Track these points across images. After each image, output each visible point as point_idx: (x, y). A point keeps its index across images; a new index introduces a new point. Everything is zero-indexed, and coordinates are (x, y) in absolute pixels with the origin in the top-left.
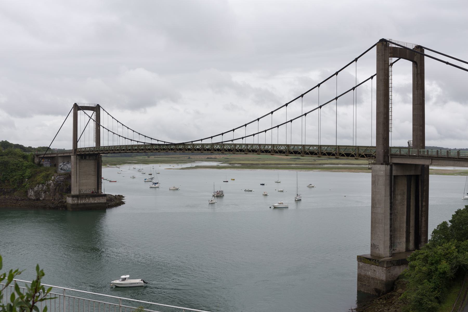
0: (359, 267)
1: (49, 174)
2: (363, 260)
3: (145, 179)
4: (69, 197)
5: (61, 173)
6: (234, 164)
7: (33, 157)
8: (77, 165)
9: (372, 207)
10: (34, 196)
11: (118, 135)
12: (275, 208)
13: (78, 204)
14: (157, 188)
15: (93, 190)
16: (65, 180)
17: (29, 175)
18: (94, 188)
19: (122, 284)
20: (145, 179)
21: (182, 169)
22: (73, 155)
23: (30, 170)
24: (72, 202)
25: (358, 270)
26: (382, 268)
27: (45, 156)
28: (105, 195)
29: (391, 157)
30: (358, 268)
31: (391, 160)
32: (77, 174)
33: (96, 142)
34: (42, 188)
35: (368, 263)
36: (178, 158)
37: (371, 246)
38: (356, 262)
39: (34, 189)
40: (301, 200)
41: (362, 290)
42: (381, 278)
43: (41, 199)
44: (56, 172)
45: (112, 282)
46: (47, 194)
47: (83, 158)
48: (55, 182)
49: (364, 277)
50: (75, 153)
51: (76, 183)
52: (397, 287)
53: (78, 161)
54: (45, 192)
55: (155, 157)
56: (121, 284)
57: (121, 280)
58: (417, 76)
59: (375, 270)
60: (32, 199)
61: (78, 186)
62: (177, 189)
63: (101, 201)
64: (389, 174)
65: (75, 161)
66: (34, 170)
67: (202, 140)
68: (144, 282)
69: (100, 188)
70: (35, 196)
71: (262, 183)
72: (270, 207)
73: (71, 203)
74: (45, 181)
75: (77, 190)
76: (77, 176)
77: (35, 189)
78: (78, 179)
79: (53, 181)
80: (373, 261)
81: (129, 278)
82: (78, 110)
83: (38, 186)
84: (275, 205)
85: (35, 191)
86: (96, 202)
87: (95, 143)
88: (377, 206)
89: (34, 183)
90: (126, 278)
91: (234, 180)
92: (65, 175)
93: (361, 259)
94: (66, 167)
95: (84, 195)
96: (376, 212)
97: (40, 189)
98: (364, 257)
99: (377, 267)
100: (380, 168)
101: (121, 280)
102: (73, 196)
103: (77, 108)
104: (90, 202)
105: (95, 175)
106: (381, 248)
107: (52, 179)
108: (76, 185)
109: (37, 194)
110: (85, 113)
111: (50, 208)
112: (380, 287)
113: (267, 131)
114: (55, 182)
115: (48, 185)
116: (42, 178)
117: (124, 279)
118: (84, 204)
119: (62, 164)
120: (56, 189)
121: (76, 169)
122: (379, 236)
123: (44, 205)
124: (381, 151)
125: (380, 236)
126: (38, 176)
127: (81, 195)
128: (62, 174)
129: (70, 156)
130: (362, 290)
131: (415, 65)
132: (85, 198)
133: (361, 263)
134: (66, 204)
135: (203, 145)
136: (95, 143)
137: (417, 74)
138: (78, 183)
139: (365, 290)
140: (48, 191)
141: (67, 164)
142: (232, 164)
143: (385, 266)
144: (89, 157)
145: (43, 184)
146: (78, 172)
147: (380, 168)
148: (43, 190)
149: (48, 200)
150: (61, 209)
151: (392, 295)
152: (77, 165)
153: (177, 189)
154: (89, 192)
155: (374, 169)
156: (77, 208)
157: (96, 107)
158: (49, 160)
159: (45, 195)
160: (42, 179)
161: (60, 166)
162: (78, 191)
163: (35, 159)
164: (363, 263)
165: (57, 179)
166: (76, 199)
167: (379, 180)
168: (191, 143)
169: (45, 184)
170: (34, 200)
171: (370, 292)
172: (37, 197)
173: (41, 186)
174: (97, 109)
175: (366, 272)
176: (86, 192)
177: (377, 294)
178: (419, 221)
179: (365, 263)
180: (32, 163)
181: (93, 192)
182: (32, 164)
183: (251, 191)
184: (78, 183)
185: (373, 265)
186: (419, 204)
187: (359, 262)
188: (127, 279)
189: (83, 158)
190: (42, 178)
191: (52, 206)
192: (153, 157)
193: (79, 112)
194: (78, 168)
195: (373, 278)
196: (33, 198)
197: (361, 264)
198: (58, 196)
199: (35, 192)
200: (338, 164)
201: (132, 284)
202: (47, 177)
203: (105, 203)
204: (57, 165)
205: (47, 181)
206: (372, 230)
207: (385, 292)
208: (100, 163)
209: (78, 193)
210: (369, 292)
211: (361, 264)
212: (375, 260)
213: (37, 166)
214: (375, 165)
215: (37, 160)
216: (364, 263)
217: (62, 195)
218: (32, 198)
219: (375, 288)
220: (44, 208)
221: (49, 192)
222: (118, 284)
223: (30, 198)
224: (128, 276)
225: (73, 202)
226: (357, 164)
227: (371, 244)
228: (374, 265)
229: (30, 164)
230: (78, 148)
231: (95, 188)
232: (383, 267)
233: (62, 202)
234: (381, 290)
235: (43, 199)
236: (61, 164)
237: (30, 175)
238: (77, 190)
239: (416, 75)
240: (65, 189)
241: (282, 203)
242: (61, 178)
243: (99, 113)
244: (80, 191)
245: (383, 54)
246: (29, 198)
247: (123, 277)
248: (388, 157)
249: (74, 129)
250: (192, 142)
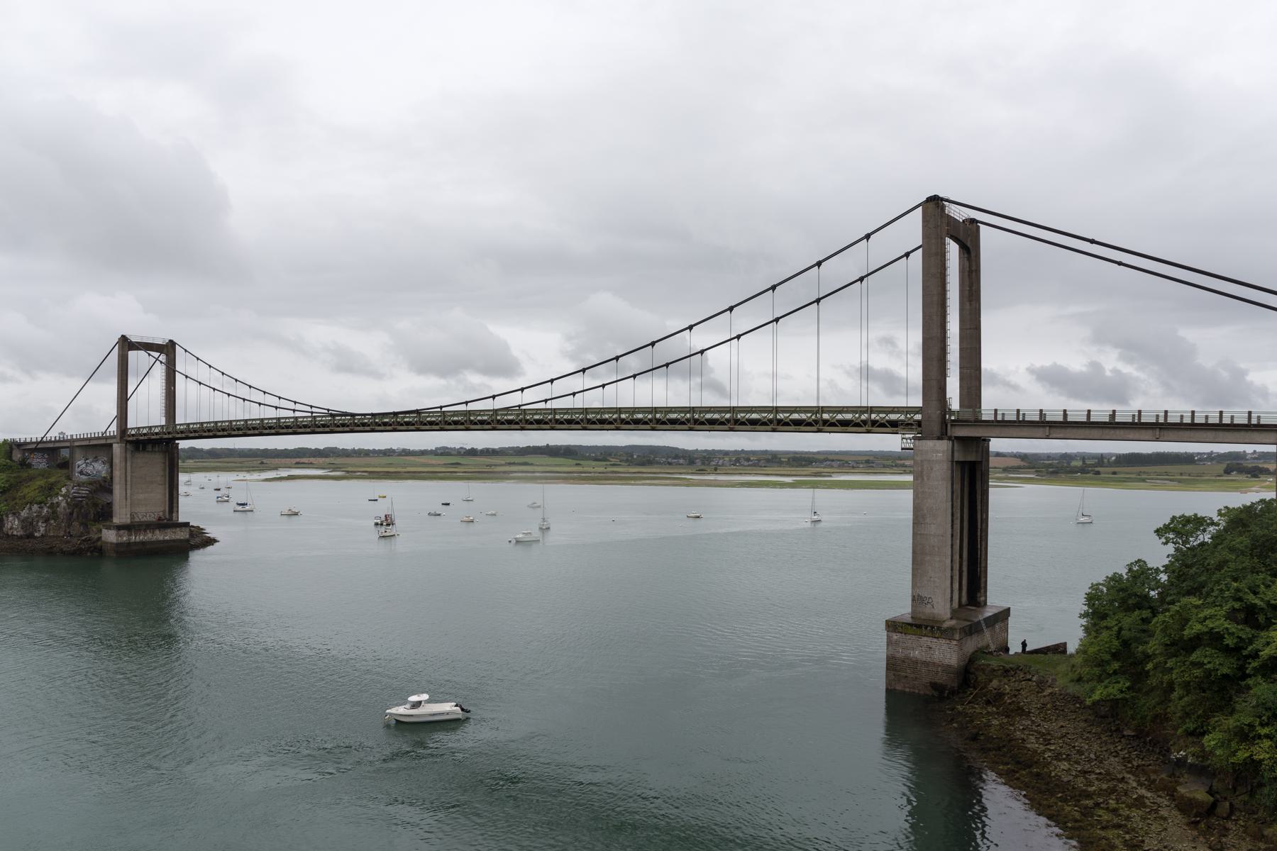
0: (890, 642)
1: (55, 482)
2: (902, 627)
3: (218, 498)
4: (108, 528)
5: (81, 480)
6: (355, 472)
7: (8, 448)
9: (913, 523)
12: (518, 542)
13: (129, 544)
14: (248, 513)
15: (161, 514)
16: (90, 495)
17: (3, 485)
18: (162, 509)
19: (412, 715)
20: (218, 498)
21: (267, 480)
22: (118, 443)
23: (5, 475)
24: (117, 540)
25: (887, 649)
26: (948, 642)
27: (40, 446)
28: (186, 525)
29: (952, 425)
30: (888, 645)
31: (951, 430)
32: (126, 481)
33: (166, 417)
34: (40, 512)
35: (912, 634)
36: (241, 463)
37: (913, 600)
38: (883, 635)
40: (549, 528)
41: (897, 688)
42: (946, 662)
43: (36, 534)
44: (69, 478)
45: (388, 711)
46: (51, 525)
47: (141, 449)
48: (69, 500)
49: (904, 661)
50: (121, 438)
51: (124, 500)
52: (977, 678)
53: (129, 455)
54: (47, 520)
55: (195, 462)
56: (409, 716)
57: (408, 706)
58: (969, 275)
59: (931, 646)
60: (14, 535)
61: (129, 506)
62: (296, 514)
63: (178, 537)
64: (950, 458)
65: (124, 455)
66: (15, 475)
67: (467, 403)
68: (462, 710)
69: (175, 509)
70: (22, 528)
71: (444, 502)
72: (510, 541)
73: (115, 541)
74: (46, 498)
75: (126, 514)
76: (126, 484)
77: (22, 514)
78: (129, 491)
79: (64, 496)
80: (926, 628)
81: (428, 701)
82: (129, 350)
83: (30, 509)
84: (518, 536)
85: (22, 518)
86: (167, 538)
87: (164, 419)
88: (928, 520)
89: (17, 501)
90: (420, 702)
91: (385, 497)
92: (91, 484)
93: (892, 626)
94: (91, 468)
95: (141, 525)
96: (926, 533)
97: (35, 514)
98: (903, 623)
99: (935, 640)
100: (935, 445)
101: (408, 706)
102: (119, 528)
103: (126, 345)
104: (154, 538)
105: (165, 484)
106: (938, 602)
108: (124, 504)
109: (28, 524)
110: (149, 355)
111: (63, 552)
112: (942, 678)
113: (577, 395)
114: (69, 500)
115: (53, 507)
116: (37, 491)
117: (417, 705)
118: (143, 543)
119: (83, 461)
120: (71, 514)
121: (124, 471)
122: (932, 579)
123: (49, 546)
124: (935, 413)
125: (936, 579)
126: (26, 487)
127: (136, 524)
128: (84, 483)
129: (111, 445)
130: (899, 687)
131: (966, 256)
132: (145, 531)
133: (894, 634)
134: (99, 543)
135: (470, 413)
136: (164, 418)
137: (969, 272)
138: (129, 500)
139: (905, 687)
140: (53, 519)
141: (93, 462)
142: (352, 472)
143: (957, 637)
144: (153, 446)
145: (40, 503)
146: (129, 478)
147: (935, 445)
148: (42, 517)
149: (54, 536)
150: (89, 554)
151: (1000, 693)
152: (126, 463)
153: (296, 514)
154: (151, 518)
155: (920, 448)
156: (126, 553)
157: (166, 346)
158: (46, 456)
160: (39, 492)
161: (78, 467)
162: (129, 516)
163: (14, 452)
164: (901, 633)
165: (74, 493)
166: (126, 532)
167: (932, 469)
168: (439, 410)
169: (45, 504)
170: (21, 537)
171: (919, 690)
172: (28, 532)
173: (35, 507)
174: (168, 350)
175: (909, 651)
176: (145, 519)
177: (936, 694)
178: (977, 549)
179: (905, 634)
180: (8, 461)
181: (160, 519)
182: (7, 463)
183: (439, 515)
184: (129, 500)
185: (927, 636)
186: (977, 516)
187: (892, 632)
188: (423, 703)
189: (141, 449)
190: (37, 491)
191: (65, 548)
192: (191, 461)
193: (132, 355)
194: (129, 468)
195: (926, 664)
196: (18, 532)
197: (895, 637)
198: (76, 527)
199: (23, 521)
200: (533, 472)
201: (434, 715)
202: (51, 489)
203: (187, 541)
204: (72, 464)
205: (51, 496)
206: (913, 569)
207: (956, 688)
208: (176, 460)
209: (129, 521)
210: (917, 691)
211: (896, 637)
212: (932, 627)
213: (20, 467)
214: (921, 441)
215: (17, 456)
216: (903, 635)
217: (85, 525)
218: (15, 533)
219: (931, 683)
220: (50, 553)
221: (55, 520)
222: (401, 717)
223: (10, 533)
224: (425, 697)
225: (120, 538)
226: (565, 473)
227: (913, 597)
228: (929, 637)
229: (4, 463)
230: (128, 427)
231: (165, 510)
232: (950, 639)
233: (89, 540)
234: (946, 685)
235: (42, 535)
236: (79, 463)
237: (7, 485)
238: (126, 514)
239: (967, 273)
240: (92, 512)
241: (530, 533)
242: (83, 490)
243: (173, 357)
244: (132, 516)
245: (939, 224)
246: (8, 534)
247: (414, 698)
248: (946, 426)
249: (121, 389)
250: (441, 407)
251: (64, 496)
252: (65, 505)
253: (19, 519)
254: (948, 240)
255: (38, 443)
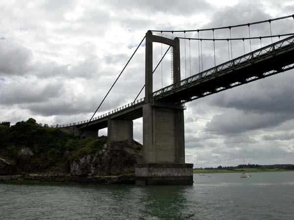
8: (152, 116)
10: (80, 171)
11: (199, 39)
39: (80, 161)
46: (98, 167)
53: (154, 112)
63: (186, 174)
86: (179, 175)
107: (105, 147)
120: (111, 160)
138: (154, 145)
146: (154, 129)
152: (152, 116)
159: (95, 169)
193: (156, 45)
218: (77, 174)
251: (106, 149)
252: (107, 154)
253: (79, 164)
254: (142, 144)
255: (88, 123)
